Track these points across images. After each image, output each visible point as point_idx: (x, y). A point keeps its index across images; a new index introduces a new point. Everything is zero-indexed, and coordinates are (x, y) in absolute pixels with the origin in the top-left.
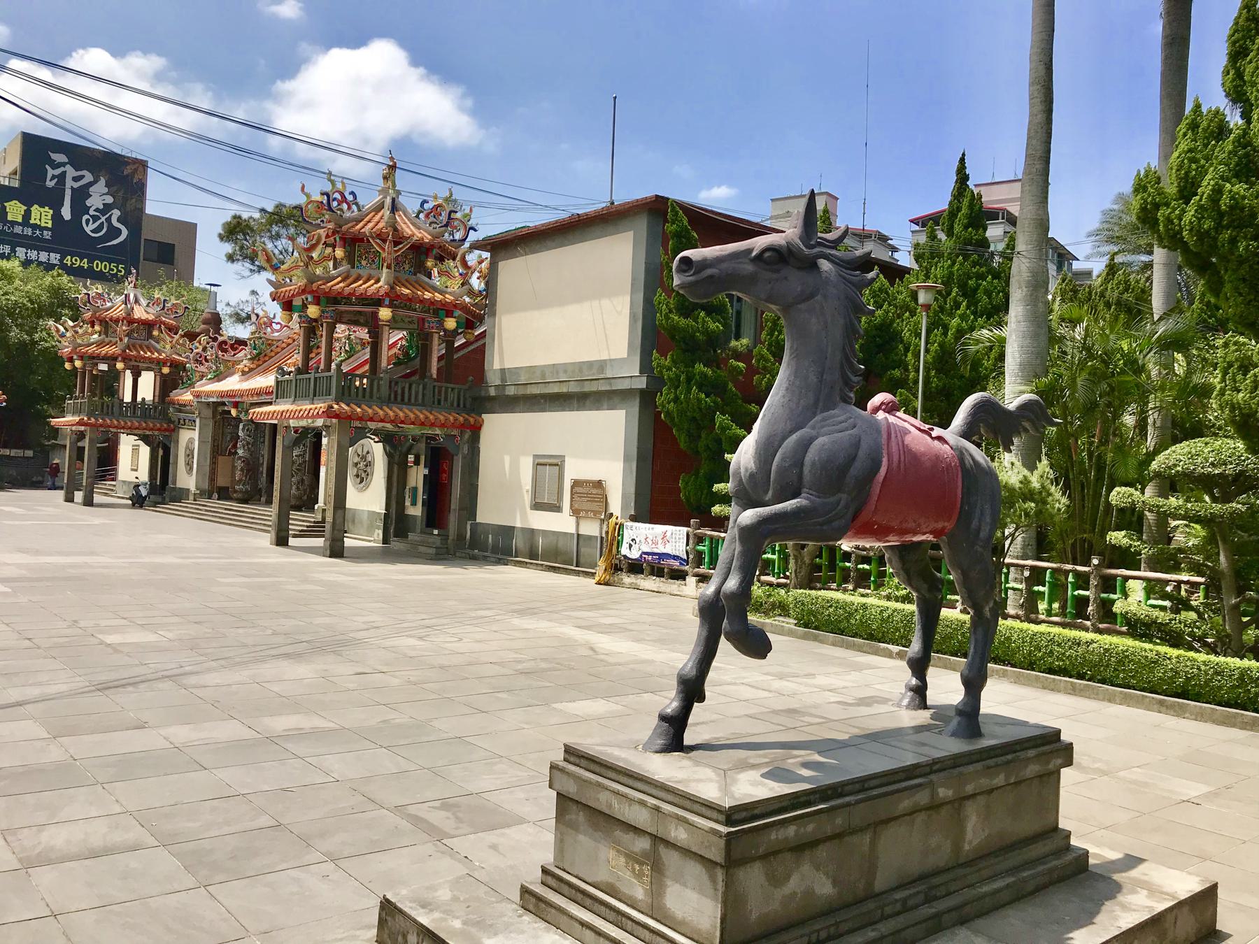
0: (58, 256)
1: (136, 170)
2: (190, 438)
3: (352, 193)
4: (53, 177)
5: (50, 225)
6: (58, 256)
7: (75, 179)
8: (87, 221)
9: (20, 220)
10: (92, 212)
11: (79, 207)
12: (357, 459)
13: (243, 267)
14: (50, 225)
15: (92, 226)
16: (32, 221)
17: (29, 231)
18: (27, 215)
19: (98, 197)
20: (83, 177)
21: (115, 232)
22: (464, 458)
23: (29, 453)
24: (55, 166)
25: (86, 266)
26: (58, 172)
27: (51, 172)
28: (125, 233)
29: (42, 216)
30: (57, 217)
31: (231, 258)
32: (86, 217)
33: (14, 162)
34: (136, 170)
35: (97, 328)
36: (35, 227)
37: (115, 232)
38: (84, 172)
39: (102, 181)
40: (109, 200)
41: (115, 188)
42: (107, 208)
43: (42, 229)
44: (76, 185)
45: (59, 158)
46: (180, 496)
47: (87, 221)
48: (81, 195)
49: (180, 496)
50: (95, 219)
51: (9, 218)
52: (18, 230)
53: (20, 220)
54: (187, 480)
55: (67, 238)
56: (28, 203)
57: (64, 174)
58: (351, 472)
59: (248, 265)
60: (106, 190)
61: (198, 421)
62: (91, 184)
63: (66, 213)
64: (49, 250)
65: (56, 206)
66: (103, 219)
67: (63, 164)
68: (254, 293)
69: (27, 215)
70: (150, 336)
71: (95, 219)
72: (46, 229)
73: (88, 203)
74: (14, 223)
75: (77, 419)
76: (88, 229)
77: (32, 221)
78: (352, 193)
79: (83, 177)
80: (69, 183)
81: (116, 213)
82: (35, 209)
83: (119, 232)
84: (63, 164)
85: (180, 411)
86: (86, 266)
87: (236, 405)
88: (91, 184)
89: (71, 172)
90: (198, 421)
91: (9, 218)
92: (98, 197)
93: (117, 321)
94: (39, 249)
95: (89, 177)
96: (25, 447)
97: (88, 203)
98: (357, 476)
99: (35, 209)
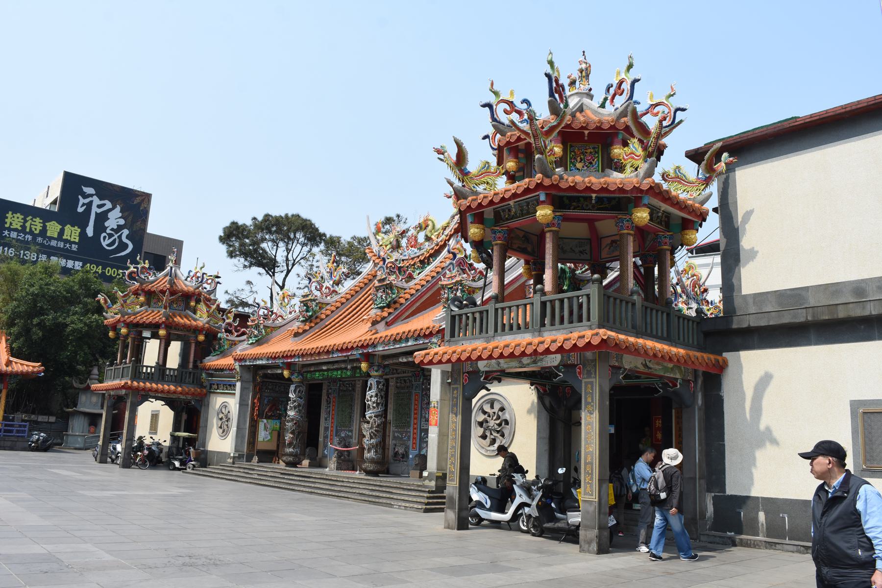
0: (81, 264)
1: (143, 200)
2: (228, 404)
3: (525, 101)
4: (83, 205)
5: (77, 241)
6: (81, 264)
7: (99, 206)
8: (105, 238)
9: (56, 236)
10: (108, 231)
11: (100, 227)
12: (481, 417)
13: (240, 261)
14: (77, 241)
15: (108, 241)
16: (65, 237)
17: (61, 245)
18: (62, 232)
19: (115, 219)
20: (104, 205)
21: (123, 246)
22: (700, 409)
23: (52, 419)
24: (85, 196)
25: (100, 272)
26: (87, 201)
27: (82, 201)
28: (131, 247)
29: (72, 233)
30: (83, 234)
31: (231, 255)
32: (104, 234)
33: (56, 192)
34: (143, 200)
35: (142, 299)
36: (66, 241)
37: (123, 246)
38: (106, 202)
39: (118, 208)
40: (122, 222)
41: (126, 214)
42: (120, 228)
43: (71, 243)
44: (99, 211)
45: (89, 190)
46: (204, 460)
47: (105, 238)
48: (102, 218)
49: (204, 460)
50: (110, 236)
51: (48, 234)
52: (53, 243)
53: (56, 236)
54: (221, 442)
55: (88, 249)
56: (63, 224)
57: (91, 202)
58: (476, 431)
59: (242, 260)
60: (120, 215)
61: (238, 385)
62: (110, 210)
63: (90, 231)
64: (75, 259)
65: (83, 226)
66: (116, 236)
67: (91, 195)
68: (249, 283)
69: (62, 232)
70: (187, 307)
71: (110, 236)
72: (74, 243)
73: (106, 224)
74: (51, 238)
75: (123, 382)
76: (104, 244)
77: (65, 237)
78: (525, 101)
79: (104, 205)
80: (95, 210)
81: (126, 232)
82: (68, 228)
83: (126, 246)
84: (91, 195)
85: (212, 375)
86: (100, 272)
87: (289, 366)
88: (110, 210)
89: (96, 201)
90: (238, 385)
91: (48, 234)
92: (115, 219)
93: (163, 292)
94: (67, 258)
95: (109, 205)
96: (50, 414)
97: (106, 224)
98: (484, 437)
99: (68, 228)
